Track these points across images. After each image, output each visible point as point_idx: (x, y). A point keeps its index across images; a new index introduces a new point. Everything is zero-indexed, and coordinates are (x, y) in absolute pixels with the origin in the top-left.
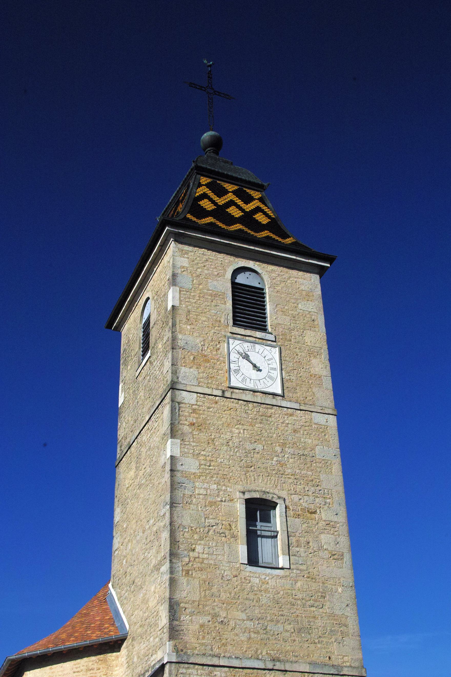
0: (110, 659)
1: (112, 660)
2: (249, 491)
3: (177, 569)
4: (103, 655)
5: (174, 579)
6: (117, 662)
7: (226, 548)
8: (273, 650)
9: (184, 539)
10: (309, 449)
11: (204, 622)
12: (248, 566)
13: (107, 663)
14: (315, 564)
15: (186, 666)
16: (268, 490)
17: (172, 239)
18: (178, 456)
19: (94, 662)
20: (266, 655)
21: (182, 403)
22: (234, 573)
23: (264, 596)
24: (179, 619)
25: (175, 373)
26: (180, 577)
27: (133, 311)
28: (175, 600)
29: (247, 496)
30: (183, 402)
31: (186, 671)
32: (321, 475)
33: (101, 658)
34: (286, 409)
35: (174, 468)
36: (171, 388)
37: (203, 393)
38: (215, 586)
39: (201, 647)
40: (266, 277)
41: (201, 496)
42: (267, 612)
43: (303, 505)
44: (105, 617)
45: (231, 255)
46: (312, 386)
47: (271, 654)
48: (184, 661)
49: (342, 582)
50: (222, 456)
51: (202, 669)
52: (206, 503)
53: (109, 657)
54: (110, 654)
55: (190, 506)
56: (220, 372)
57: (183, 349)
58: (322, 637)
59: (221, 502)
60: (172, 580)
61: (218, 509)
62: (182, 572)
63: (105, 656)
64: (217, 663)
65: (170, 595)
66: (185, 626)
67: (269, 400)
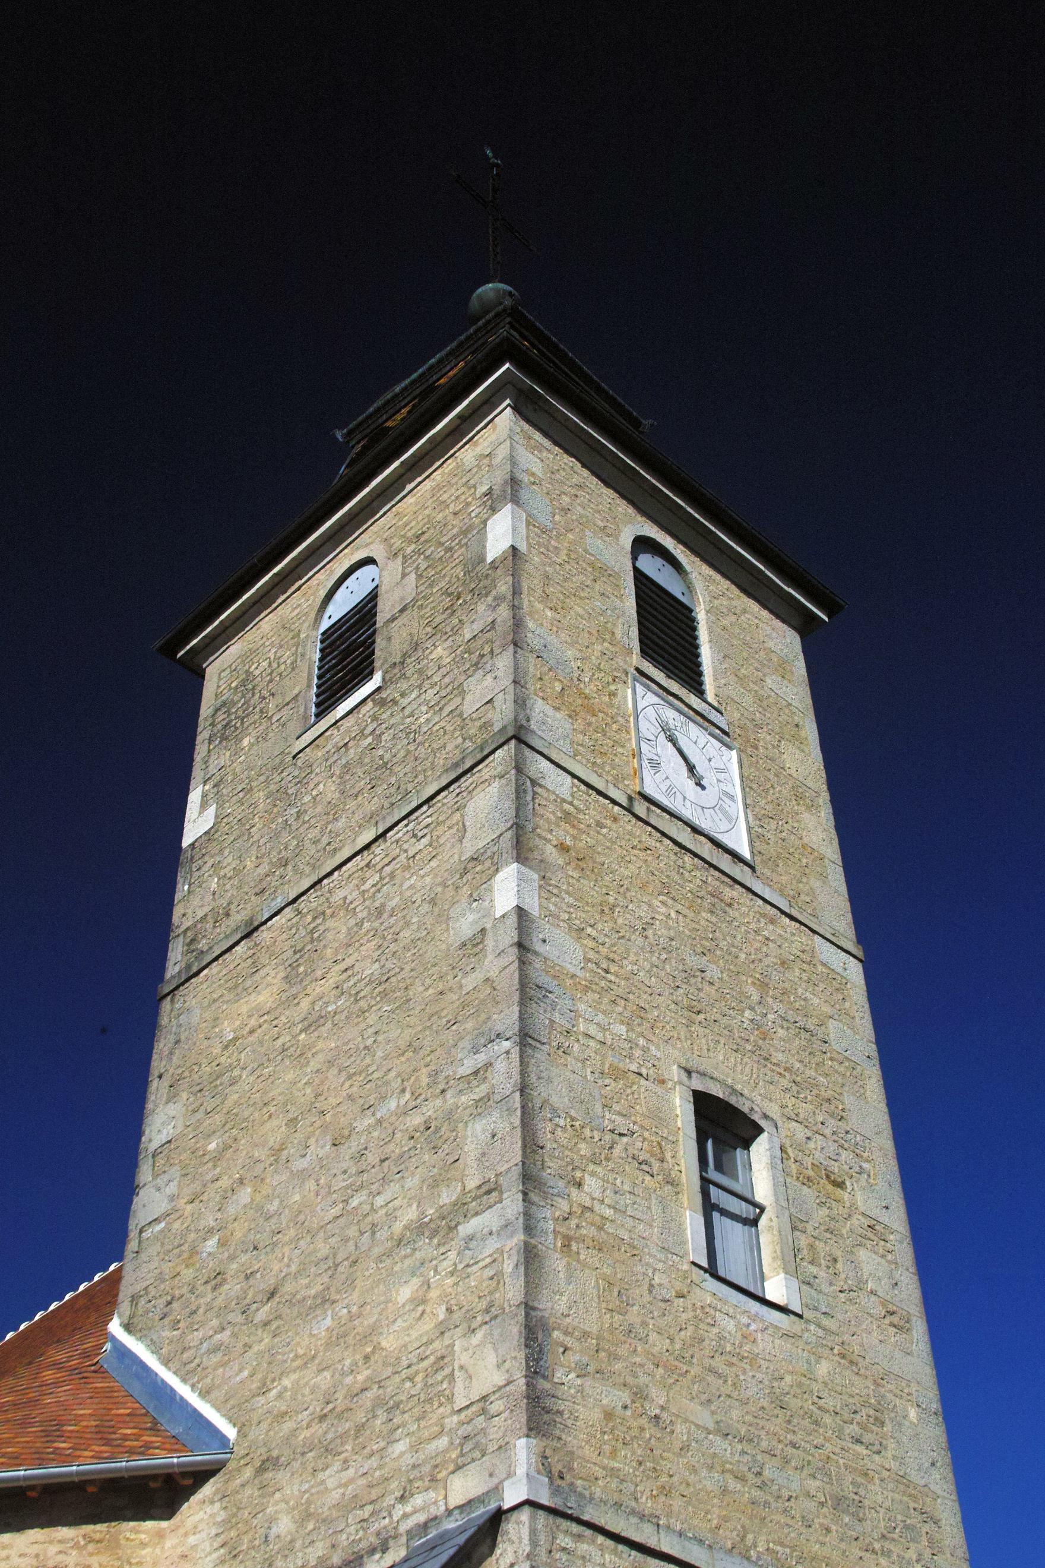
0: (133, 1540)
1: (137, 1542)
2: (703, 1074)
3: (541, 1224)
4: (106, 1525)
5: (535, 1250)
6: (158, 1551)
7: (656, 1209)
8: (782, 1544)
9: (555, 1146)
10: (816, 1021)
11: (613, 1405)
12: (707, 1275)
13: (120, 1552)
14: (853, 1323)
15: (575, 1528)
16: (738, 1087)
17: (508, 401)
18: (534, 913)
19: (69, 1545)
20: (766, 1553)
21: (541, 786)
22: (678, 1285)
23: (751, 1374)
24: (550, 1374)
25: (521, 703)
26: (550, 1251)
27: (274, 606)
28: (540, 1314)
29: (698, 1084)
30: (540, 781)
31: (574, 1546)
32: (845, 1094)
33: (95, 1532)
34: (760, 902)
35: (526, 943)
36: (514, 737)
37: (586, 780)
38: (636, 1308)
39: (608, 1479)
40: (699, 585)
41: (592, 1043)
42: (760, 1425)
43: (816, 1156)
44: (111, 1409)
45: (631, 502)
46: (807, 871)
47: (777, 1553)
48: (570, 1512)
49: (915, 1394)
50: (632, 957)
51: (614, 1552)
52: (603, 1063)
53: (128, 1535)
54: (132, 1524)
55: (566, 1060)
56: (620, 750)
57: (538, 657)
58: (887, 1539)
59: (638, 1076)
60: (530, 1252)
61: (633, 1093)
62: (555, 1239)
63: (112, 1530)
64: (652, 1543)
65: (526, 1294)
66: (567, 1403)
67: (725, 863)
